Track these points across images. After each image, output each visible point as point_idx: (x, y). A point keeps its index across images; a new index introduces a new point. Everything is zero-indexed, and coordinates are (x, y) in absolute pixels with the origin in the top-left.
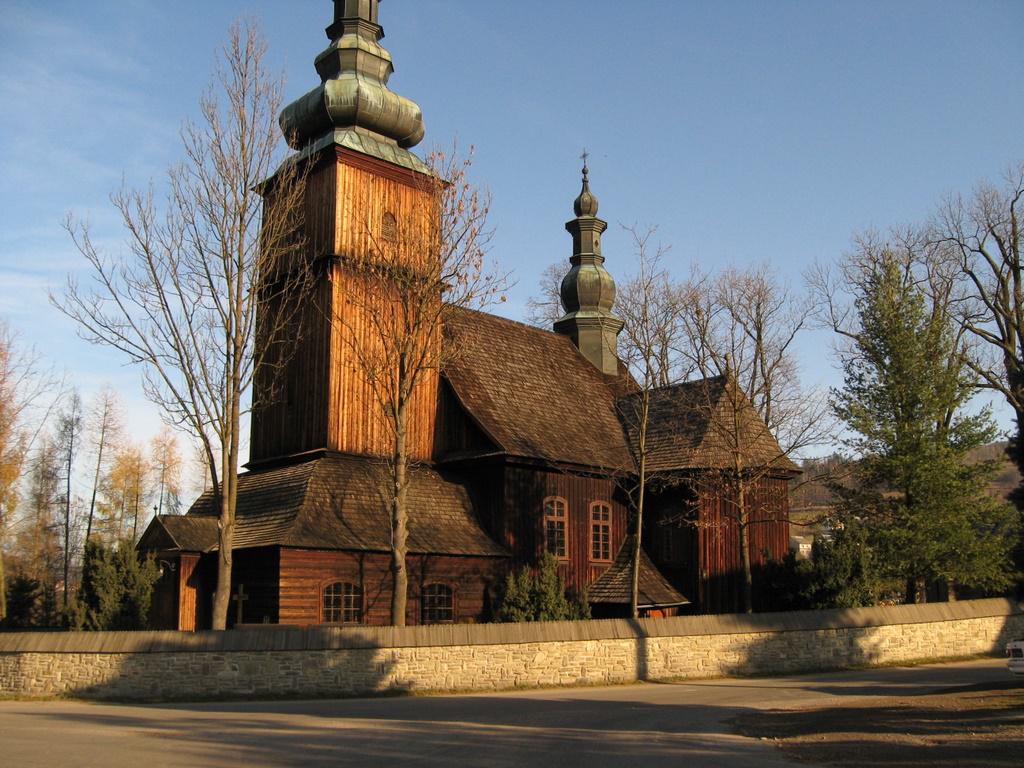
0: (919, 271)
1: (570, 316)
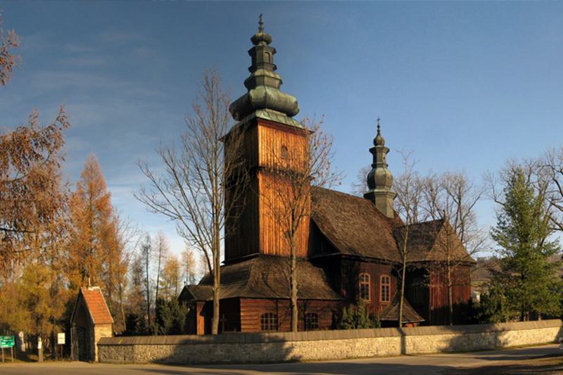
0: (534, 178)
1: (372, 191)
